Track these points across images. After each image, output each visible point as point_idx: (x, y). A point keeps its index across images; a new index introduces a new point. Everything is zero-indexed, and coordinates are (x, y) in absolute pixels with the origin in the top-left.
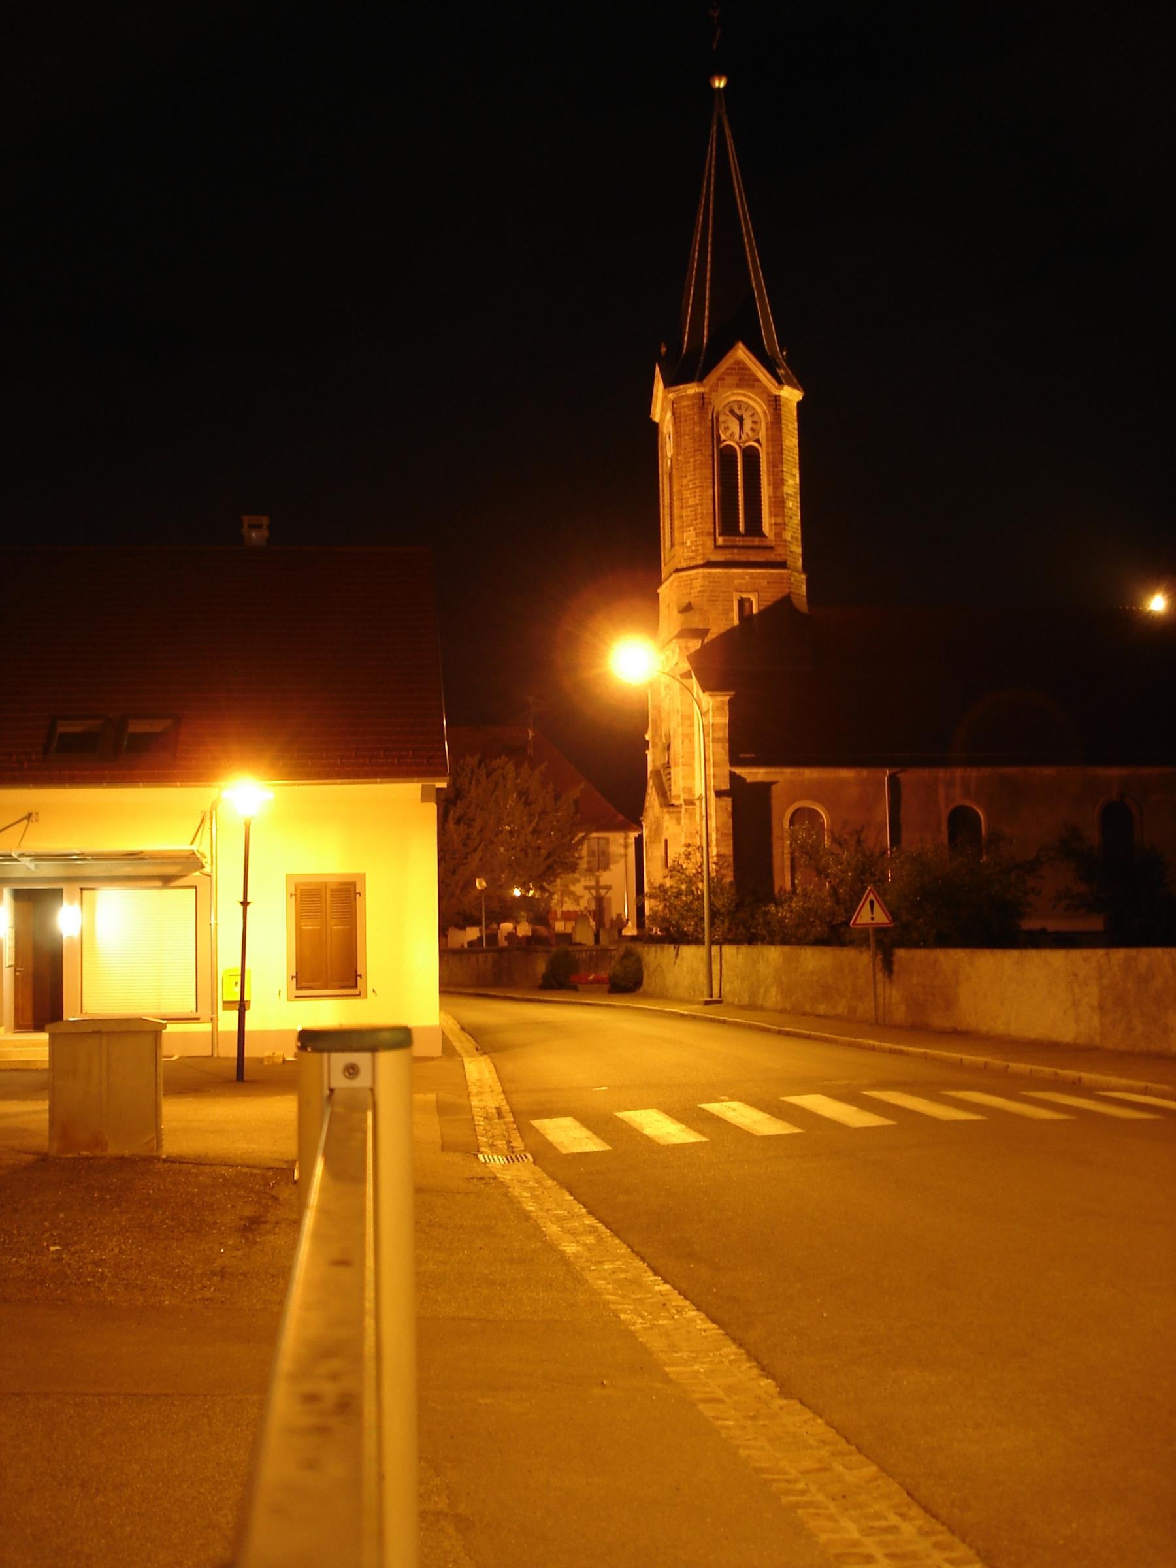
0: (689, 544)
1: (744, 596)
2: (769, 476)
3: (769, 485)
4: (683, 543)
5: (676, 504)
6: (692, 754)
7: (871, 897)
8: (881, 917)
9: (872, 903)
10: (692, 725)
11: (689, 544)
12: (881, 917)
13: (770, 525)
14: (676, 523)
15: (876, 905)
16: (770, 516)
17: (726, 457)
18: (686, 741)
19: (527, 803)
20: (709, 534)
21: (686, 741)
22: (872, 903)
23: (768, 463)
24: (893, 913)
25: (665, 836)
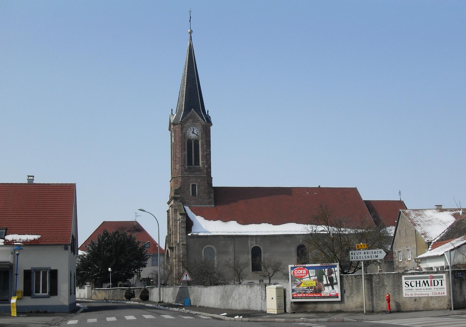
1: (194, 183)
16: (202, 160)
17: (189, 142)
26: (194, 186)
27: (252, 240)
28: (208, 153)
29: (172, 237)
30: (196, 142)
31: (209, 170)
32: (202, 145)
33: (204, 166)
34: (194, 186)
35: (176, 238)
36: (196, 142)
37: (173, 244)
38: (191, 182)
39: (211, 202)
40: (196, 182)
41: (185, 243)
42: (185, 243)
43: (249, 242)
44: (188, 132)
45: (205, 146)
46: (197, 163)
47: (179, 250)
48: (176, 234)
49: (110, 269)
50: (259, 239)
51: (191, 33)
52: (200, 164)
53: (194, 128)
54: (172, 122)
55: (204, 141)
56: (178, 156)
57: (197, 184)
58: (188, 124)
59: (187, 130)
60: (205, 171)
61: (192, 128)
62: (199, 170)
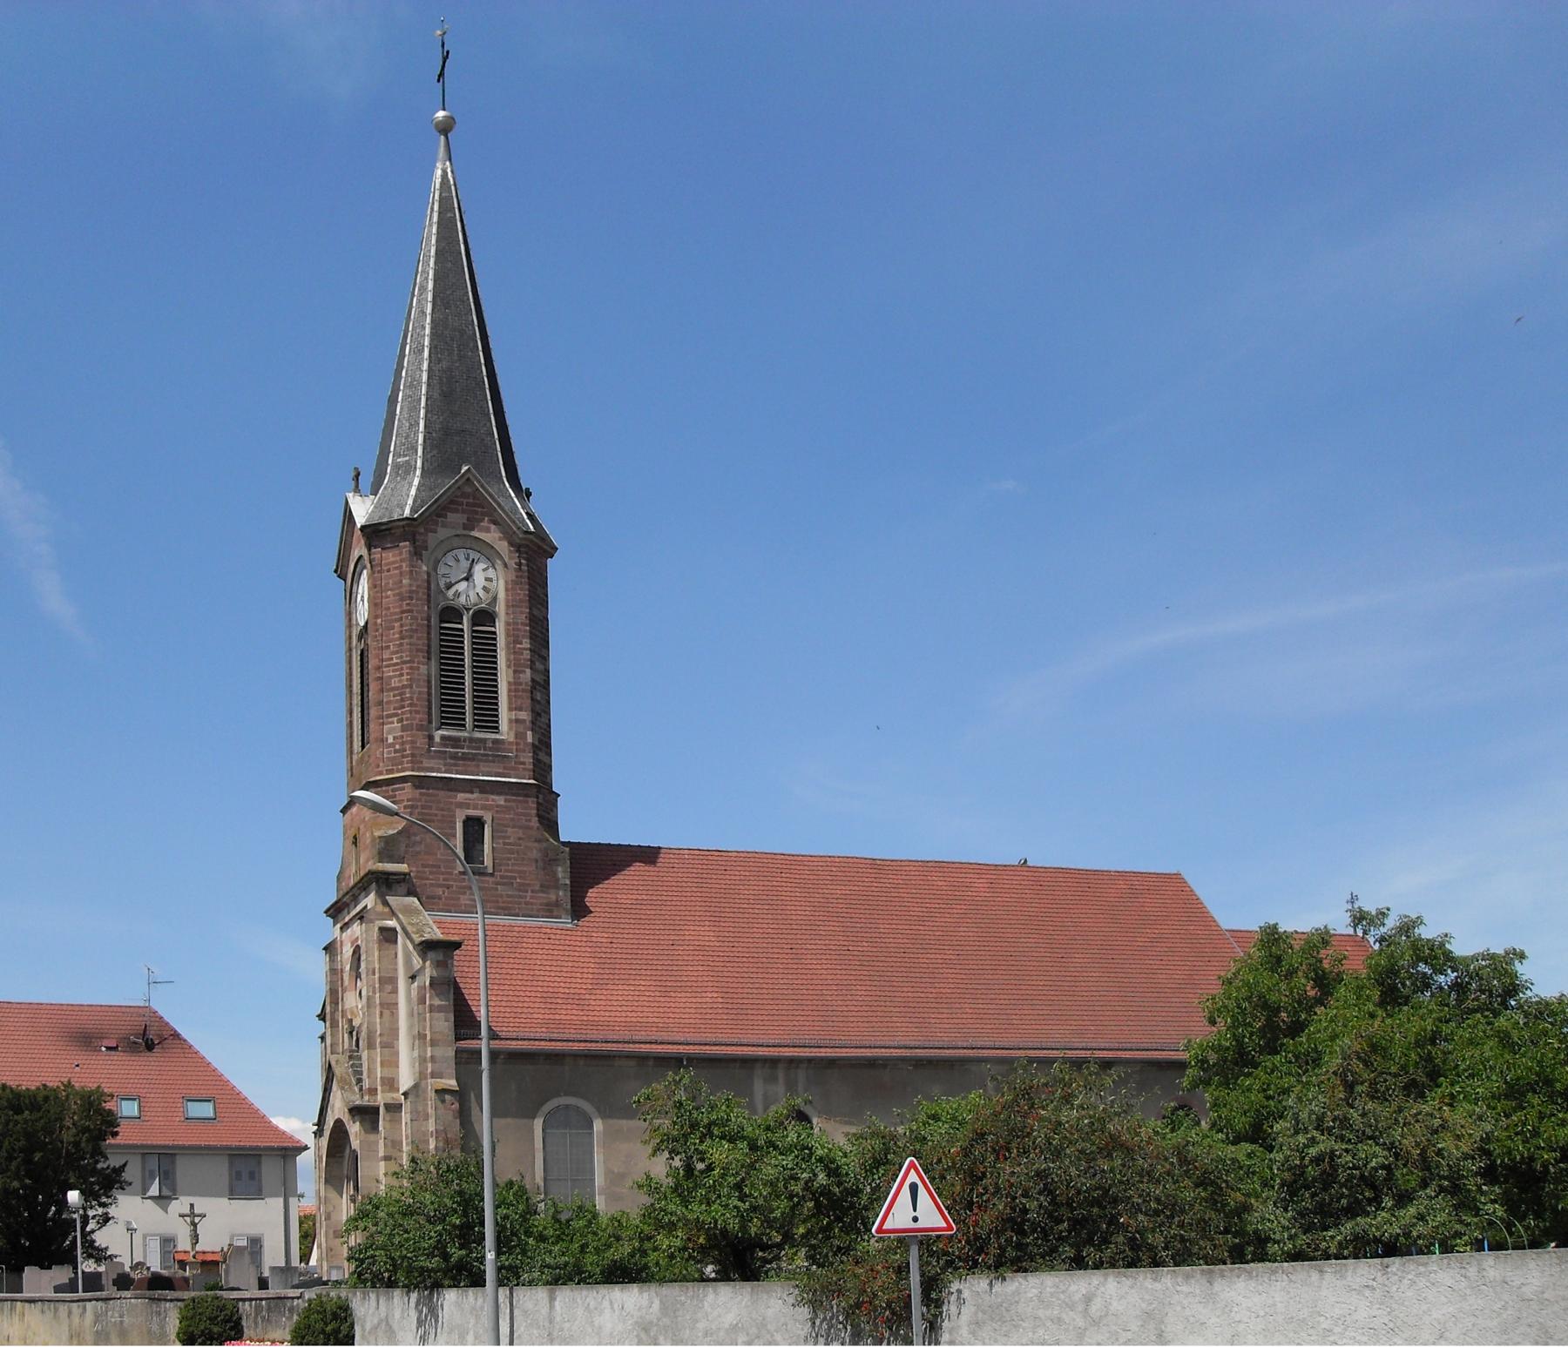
0: (391, 740)
1: (471, 812)
2: (508, 654)
3: (509, 666)
4: (383, 740)
5: (373, 687)
6: (394, 1032)
7: (913, 1177)
8: (930, 1215)
9: (914, 1189)
10: (395, 991)
11: (391, 740)
12: (930, 1215)
13: (510, 721)
14: (373, 712)
15: (922, 1191)
16: (510, 709)
17: (451, 613)
18: (387, 1013)
19: (1337, 1036)
20: (420, 728)
21: (387, 1013)
22: (914, 1189)
23: (508, 635)
24: (957, 1206)
25: (112, 1211)
26: (474, 827)
27: (772, 1079)
28: (1273, 1249)
29: (371, 1060)
30: (484, 617)
31: (542, 756)
32: (513, 639)
33: (520, 736)
34: (474, 827)
35: (391, 1062)
36: (484, 617)
37: (373, 1091)
38: (461, 805)
39: (557, 904)
40: (484, 808)
41: (452, 1083)
42: (452, 1083)
43: (759, 1087)
44: (442, 570)
45: (526, 644)
46: (487, 719)
47: (418, 1116)
48: (390, 1045)
49: (73, 1196)
50: (801, 1075)
51: (441, 75)
52: (504, 724)
53: (473, 554)
54: (360, 520)
55: (523, 618)
56: (395, 683)
57: (488, 817)
58: (443, 533)
59: (437, 562)
60: (528, 758)
61: (461, 554)
62: (496, 753)
